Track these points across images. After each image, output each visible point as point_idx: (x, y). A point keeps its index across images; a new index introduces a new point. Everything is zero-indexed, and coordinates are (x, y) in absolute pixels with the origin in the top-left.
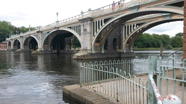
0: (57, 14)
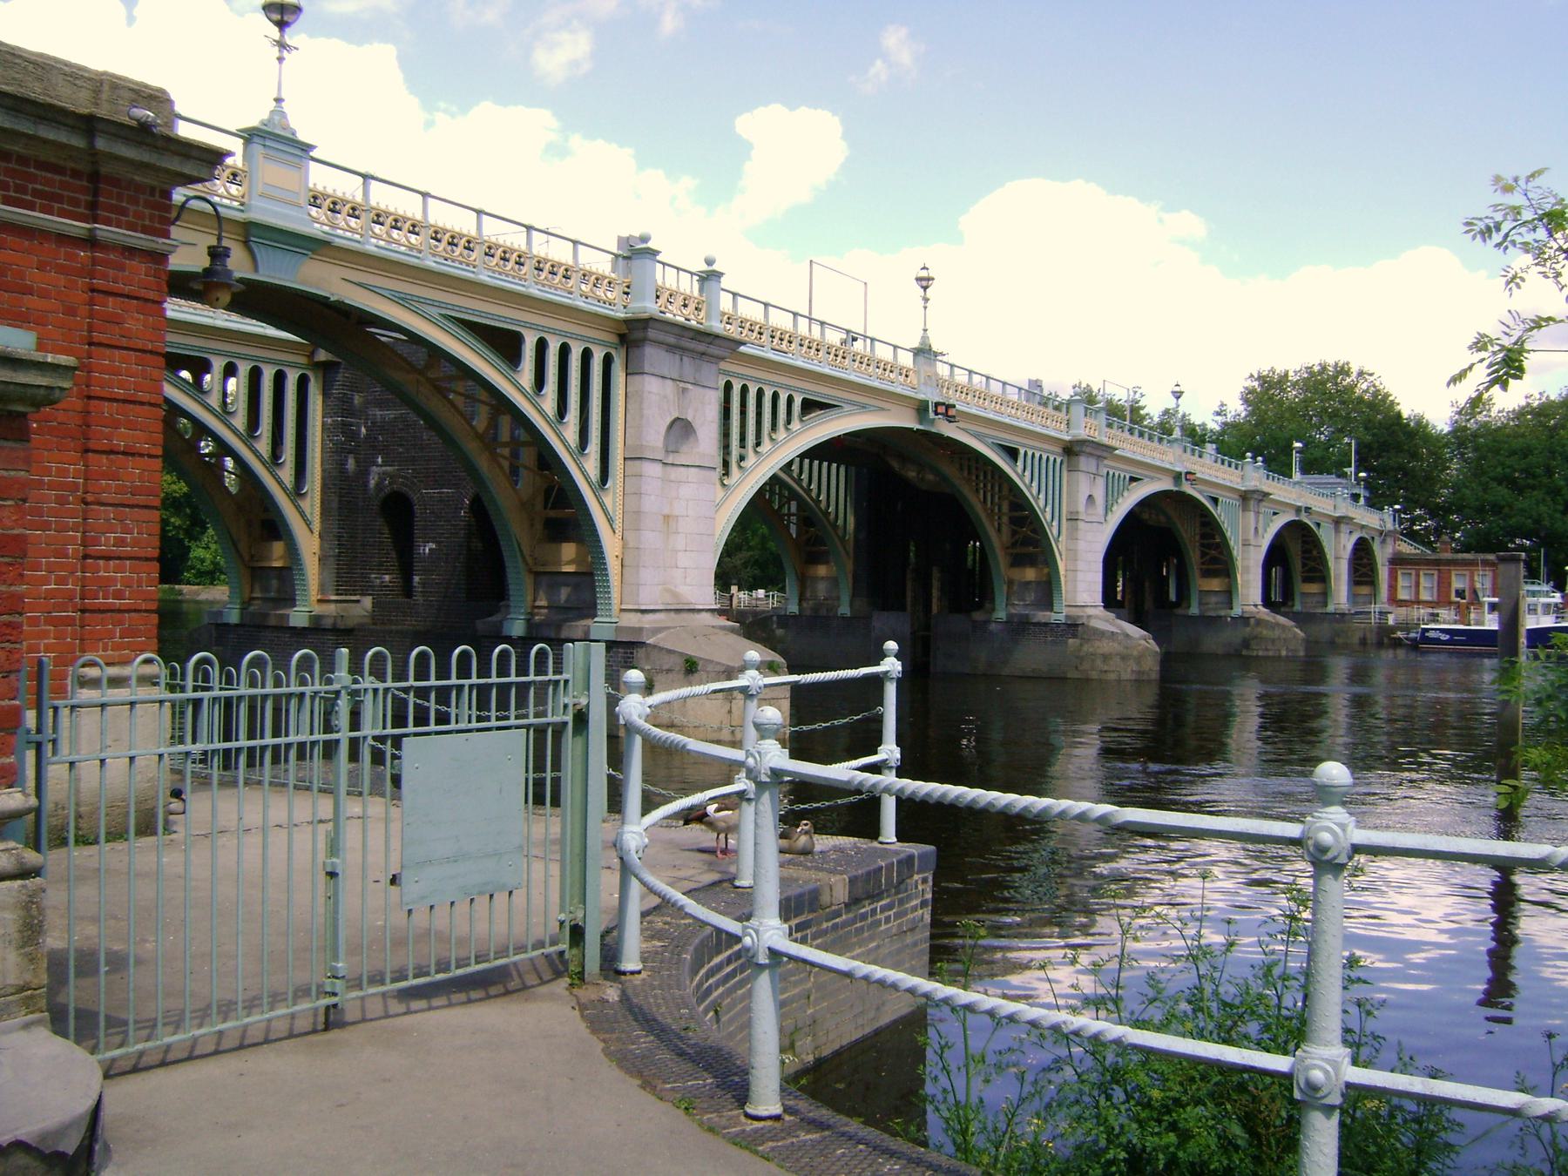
0: (925, 282)
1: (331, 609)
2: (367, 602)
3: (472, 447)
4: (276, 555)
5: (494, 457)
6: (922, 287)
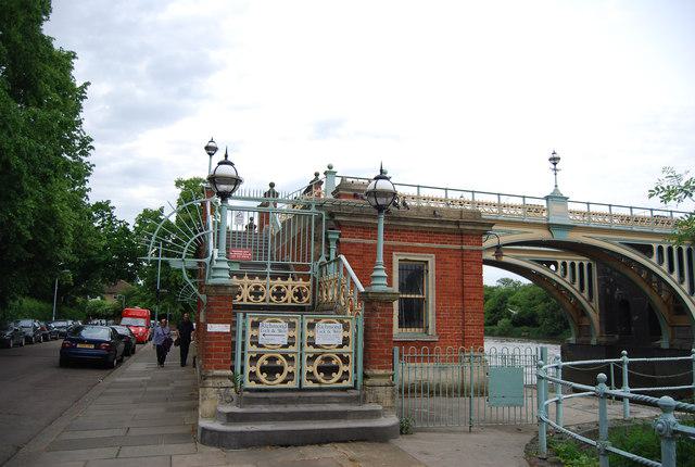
1: (603, 339)
5: (651, 287)
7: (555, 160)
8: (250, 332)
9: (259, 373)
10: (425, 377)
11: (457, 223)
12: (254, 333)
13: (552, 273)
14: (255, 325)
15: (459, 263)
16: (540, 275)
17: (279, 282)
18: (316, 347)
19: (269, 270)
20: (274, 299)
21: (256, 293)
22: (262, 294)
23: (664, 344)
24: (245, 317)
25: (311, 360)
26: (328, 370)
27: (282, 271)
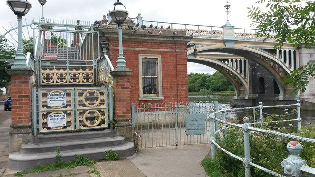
1: (251, 97)
2: (258, 95)
3: (271, 70)
4: (242, 89)
6: (16, 13)
7: (228, 7)
8: (42, 99)
9: (85, 121)
10: (157, 119)
11: (173, 37)
12: (45, 100)
13: (228, 66)
14: (45, 95)
15: (174, 59)
16: (220, 67)
17: (75, 71)
18: (48, 107)
19: (68, 65)
20: (72, 81)
21: (61, 78)
22: (52, 78)
23: (281, 98)
24: (37, 91)
25: (82, 113)
26: (91, 119)
27: (76, 65)
